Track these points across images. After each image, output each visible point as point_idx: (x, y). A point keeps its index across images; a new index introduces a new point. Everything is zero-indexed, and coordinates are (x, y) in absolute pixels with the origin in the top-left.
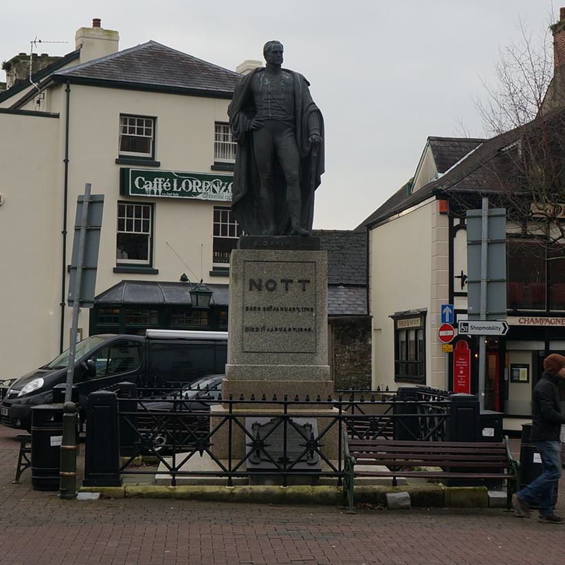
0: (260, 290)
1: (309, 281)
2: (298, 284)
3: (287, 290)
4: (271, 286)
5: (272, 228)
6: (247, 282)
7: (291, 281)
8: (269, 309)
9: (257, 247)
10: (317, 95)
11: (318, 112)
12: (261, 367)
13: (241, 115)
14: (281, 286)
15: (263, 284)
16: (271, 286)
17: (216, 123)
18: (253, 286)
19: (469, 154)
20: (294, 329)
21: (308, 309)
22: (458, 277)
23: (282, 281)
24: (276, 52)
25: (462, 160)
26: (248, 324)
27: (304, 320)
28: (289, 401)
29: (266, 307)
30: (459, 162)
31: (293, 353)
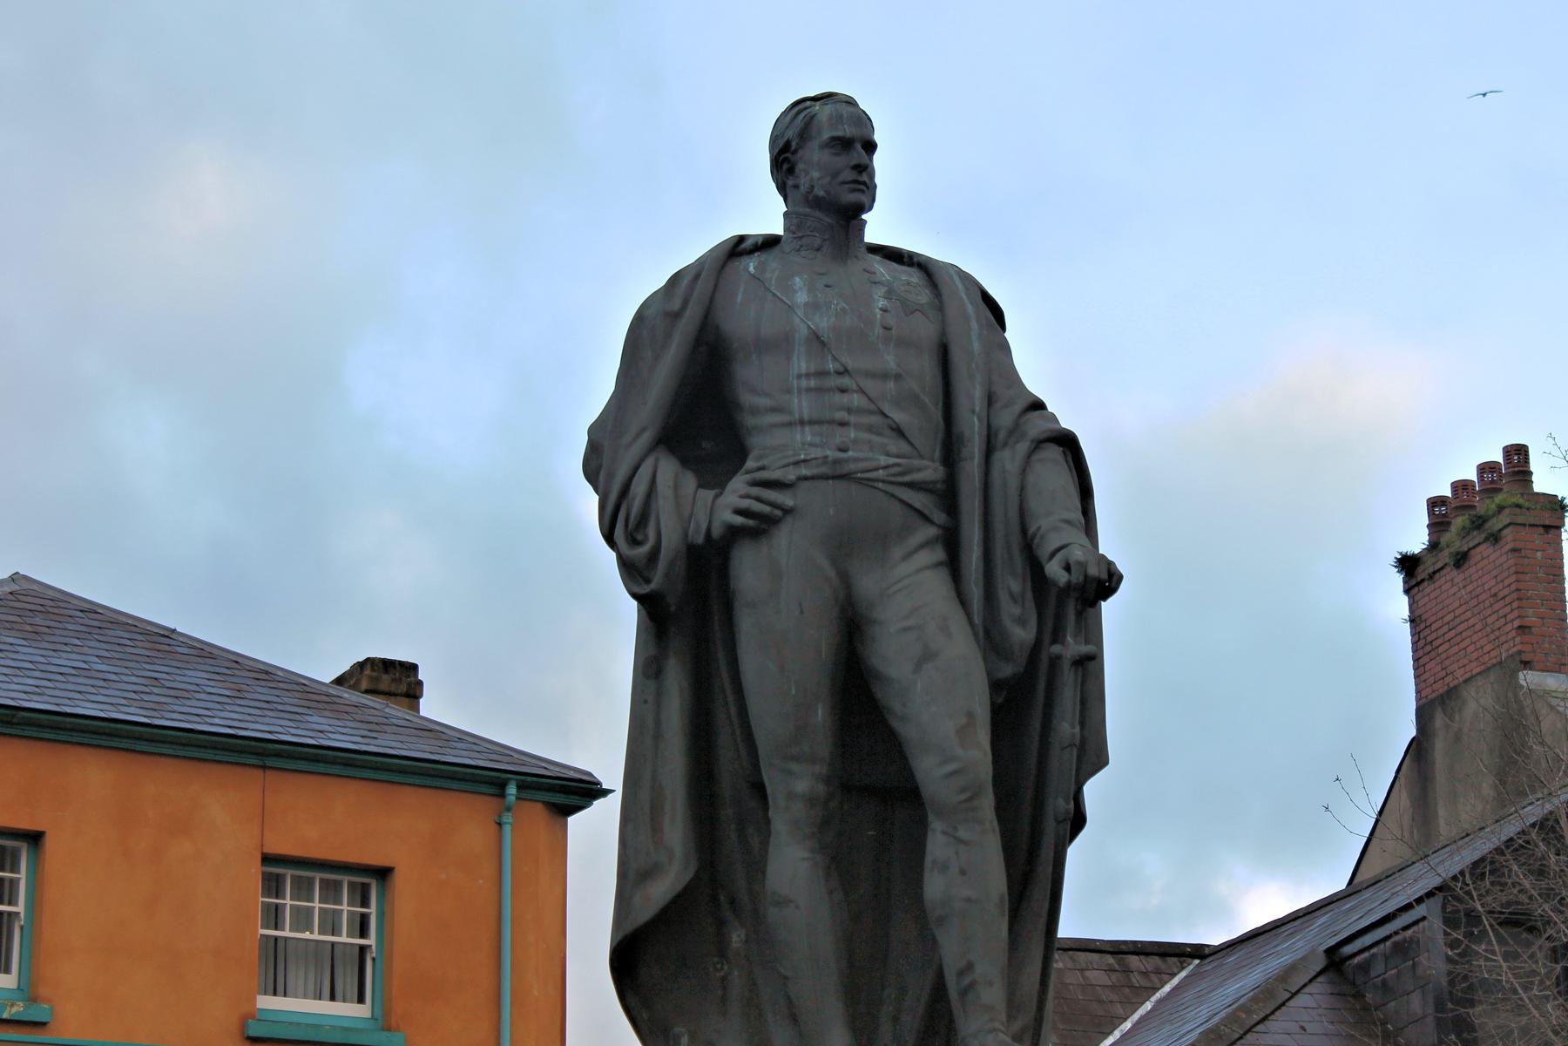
10: (1042, 360)
11: (1068, 443)
13: (668, 468)
17: (267, 859)
19: (1158, 995)
24: (844, 144)
25: (1136, 1016)
30: (1127, 1025)
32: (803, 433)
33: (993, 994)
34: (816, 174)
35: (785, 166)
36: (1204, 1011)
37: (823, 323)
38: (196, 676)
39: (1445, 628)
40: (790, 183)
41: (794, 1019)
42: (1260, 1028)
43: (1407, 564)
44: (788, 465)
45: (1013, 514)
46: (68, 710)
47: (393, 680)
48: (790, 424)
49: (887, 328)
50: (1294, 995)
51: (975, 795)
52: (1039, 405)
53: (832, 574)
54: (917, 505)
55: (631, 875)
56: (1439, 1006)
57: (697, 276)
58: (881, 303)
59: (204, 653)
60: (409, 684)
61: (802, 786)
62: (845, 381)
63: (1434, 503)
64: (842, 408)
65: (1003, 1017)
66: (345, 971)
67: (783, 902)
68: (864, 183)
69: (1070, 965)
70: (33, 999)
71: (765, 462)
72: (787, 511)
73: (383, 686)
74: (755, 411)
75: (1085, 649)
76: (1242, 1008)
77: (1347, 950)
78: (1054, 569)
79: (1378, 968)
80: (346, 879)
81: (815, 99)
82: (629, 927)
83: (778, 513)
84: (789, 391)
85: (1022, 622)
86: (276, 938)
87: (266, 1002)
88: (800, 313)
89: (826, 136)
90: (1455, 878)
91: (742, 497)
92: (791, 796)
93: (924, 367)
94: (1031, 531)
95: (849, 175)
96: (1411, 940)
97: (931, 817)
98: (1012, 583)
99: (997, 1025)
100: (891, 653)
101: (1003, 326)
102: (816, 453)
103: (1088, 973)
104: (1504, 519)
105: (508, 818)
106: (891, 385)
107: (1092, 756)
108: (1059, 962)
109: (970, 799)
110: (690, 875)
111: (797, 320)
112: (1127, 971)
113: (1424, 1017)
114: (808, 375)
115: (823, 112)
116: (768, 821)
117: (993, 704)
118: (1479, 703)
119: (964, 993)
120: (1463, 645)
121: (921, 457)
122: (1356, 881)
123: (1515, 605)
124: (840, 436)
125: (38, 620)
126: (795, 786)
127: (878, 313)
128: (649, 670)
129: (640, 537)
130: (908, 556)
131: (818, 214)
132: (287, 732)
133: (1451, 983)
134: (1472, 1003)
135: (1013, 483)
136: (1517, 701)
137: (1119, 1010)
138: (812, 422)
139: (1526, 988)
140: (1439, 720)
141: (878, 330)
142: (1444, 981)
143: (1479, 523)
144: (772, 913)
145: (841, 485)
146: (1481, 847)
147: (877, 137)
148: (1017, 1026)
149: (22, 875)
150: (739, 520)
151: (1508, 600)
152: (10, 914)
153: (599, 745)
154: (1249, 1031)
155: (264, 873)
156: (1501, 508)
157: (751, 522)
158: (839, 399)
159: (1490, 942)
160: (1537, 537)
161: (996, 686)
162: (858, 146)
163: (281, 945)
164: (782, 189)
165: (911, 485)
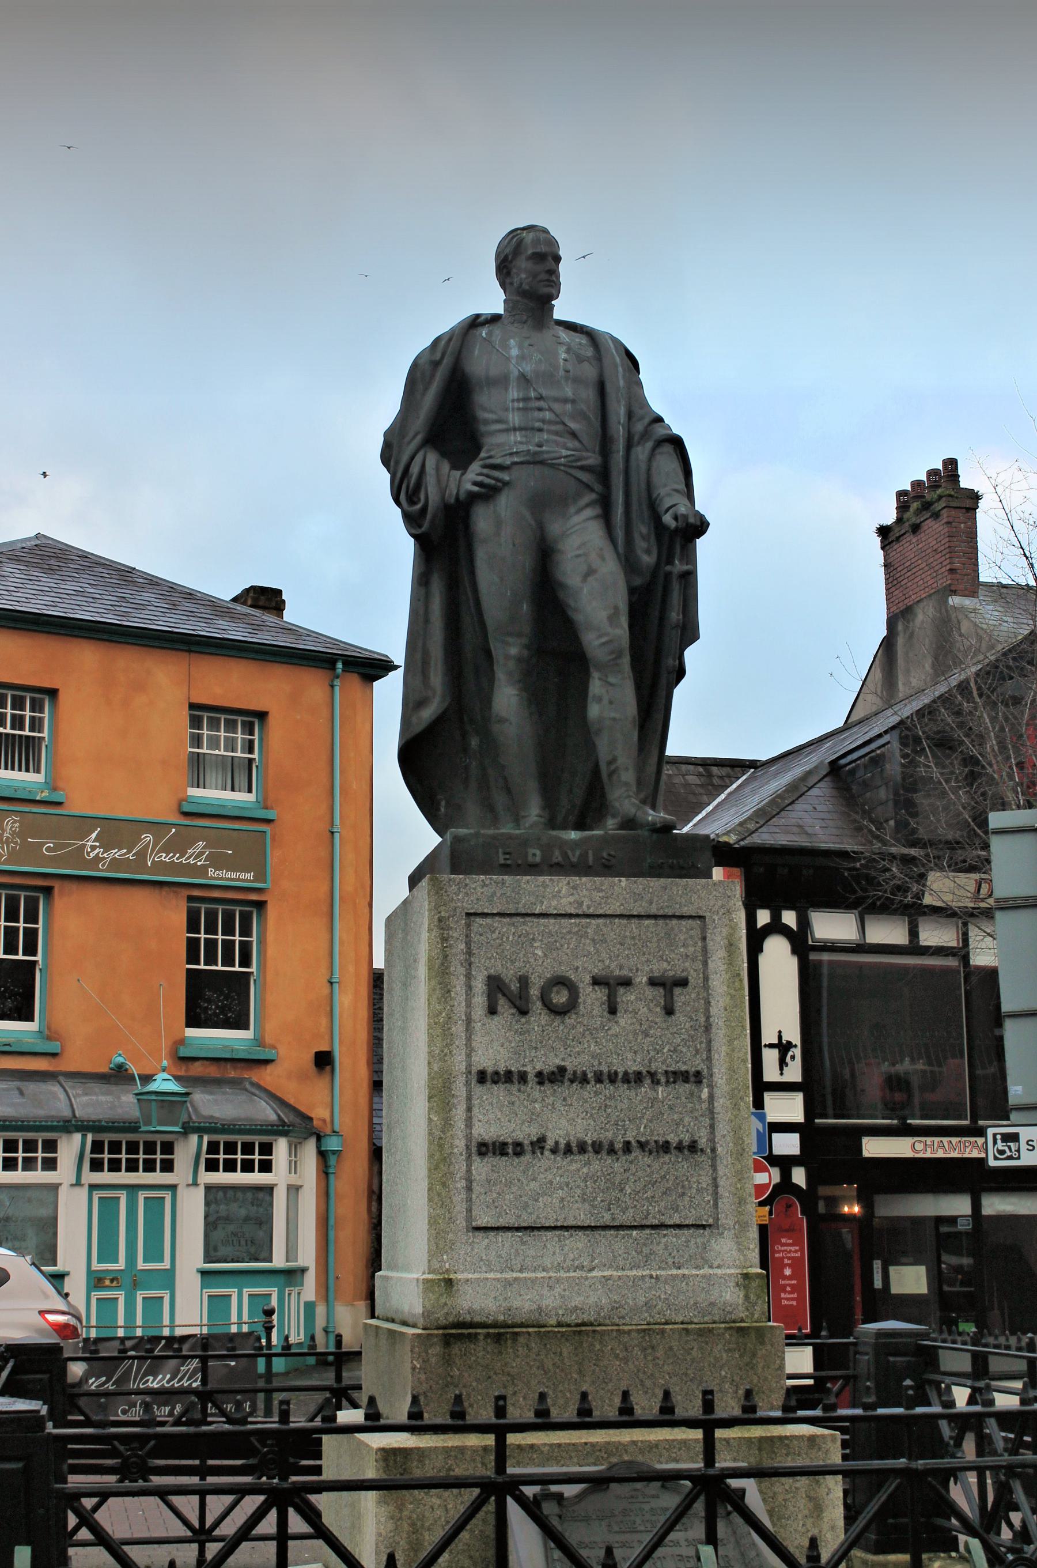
0: (523, 1012)
1: (683, 983)
2: (650, 992)
3: (613, 1011)
4: (559, 998)
5: (534, 811)
6: (479, 985)
7: (627, 983)
8: (555, 1077)
9: (506, 869)
11: (677, 443)
12: (534, 1281)
13: (432, 458)
14: (592, 998)
15: (534, 992)
16: (559, 998)
17: (193, 706)
18: (502, 1001)
19: (729, 790)
20: (642, 1145)
21: (684, 1077)
22: (771, 1046)
23: (596, 982)
25: (715, 803)
26: (485, 1130)
27: (661, 1113)
28: (720, 1413)
29: (547, 1069)
31: (643, 1227)
32: (515, 436)
33: (628, 776)
34: (523, 276)
35: (505, 271)
36: (756, 799)
37: (528, 368)
38: (148, 596)
39: (905, 571)
40: (508, 281)
41: (508, 791)
42: (789, 808)
43: (883, 531)
44: (505, 455)
45: (643, 486)
46: (72, 616)
47: (266, 599)
48: (507, 430)
49: (567, 371)
50: (810, 789)
51: (619, 655)
52: (659, 420)
53: (533, 523)
54: (585, 480)
55: (411, 704)
56: (896, 794)
57: (450, 340)
58: (564, 355)
59: (153, 582)
60: (277, 602)
61: (514, 651)
62: (542, 404)
63: (900, 494)
64: (539, 420)
65: (634, 789)
66: (239, 773)
67: (502, 720)
68: (553, 281)
69: (676, 772)
70: (55, 789)
71: (492, 453)
72: (506, 484)
73: (261, 604)
74: (487, 422)
75: (686, 568)
76: (779, 796)
77: (843, 762)
78: (668, 519)
79: (860, 773)
80: (240, 719)
81: (523, 229)
82: (409, 736)
83: (499, 484)
84: (507, 410)
85: (648, 552)
86: (198, 754)
87: (193, 792)
88: (514, 361)
89: (530, 252)
90: (908, 718)
91: (478, 475)
92: (507, 657)
93: (589, 395)
94: (654, 496)
95: (543, 276)
96: (883, 755)
97: (592, 670)
98: (642, 528)
99: (631, 794)
100: (569, 570)
101: (639, 373)
102: (524, 448)
103: (687, 777)
104: (942, 504)
105: (337, 682)
106: (569, 407)
107: (690, 633)
108: (668, 770)
109: (616, 659)
110: (446, 704)
111: (512, 366)
112: (710, 775)
113: (887, 801)
114: (518, 400)
115: (529, 237)
116: (493, 670)
117: (630, 601)
118: (924, 616)
119: (611, 774)
120: (916, 580)
121: (587, 450)
122: (850, 721)
123: (947, 556)
124: (537, 438)
125: (52, 562)
126: (509, 652)
127: (562, 362)
128: (422, 580)
129: (415, 499)
130: (579, 511)
131: (526, 301)
132: (203, 630)
133: (904, 779)
134: (916, 791)
135: (643, 467)
136: (947, 611)
137: (705, 798)
138: (520, 429)
139: (947, 782)
140: (900, 627)
141: (561, 373)
142: (899, 778)
143: (927, 506)
144: (496, 728)
145: (537, 470)
146: (926, 700)
147: (561, 253)
148: (642, 796)
149: (46, 715)
150: (476, 489)
151: (943, 553)
152: (39, 738)
153: (391, 639)
154: (783, 810)
155: (190, 715)
156: (940, 497)
157: (483, 490)
158: (536, 414)
159: (927, 757)
160: (961, 515)
161: (632, 591)
162: (550, 258)
163: (201, 757)
164: (503, 285)
165: (582, 468)
